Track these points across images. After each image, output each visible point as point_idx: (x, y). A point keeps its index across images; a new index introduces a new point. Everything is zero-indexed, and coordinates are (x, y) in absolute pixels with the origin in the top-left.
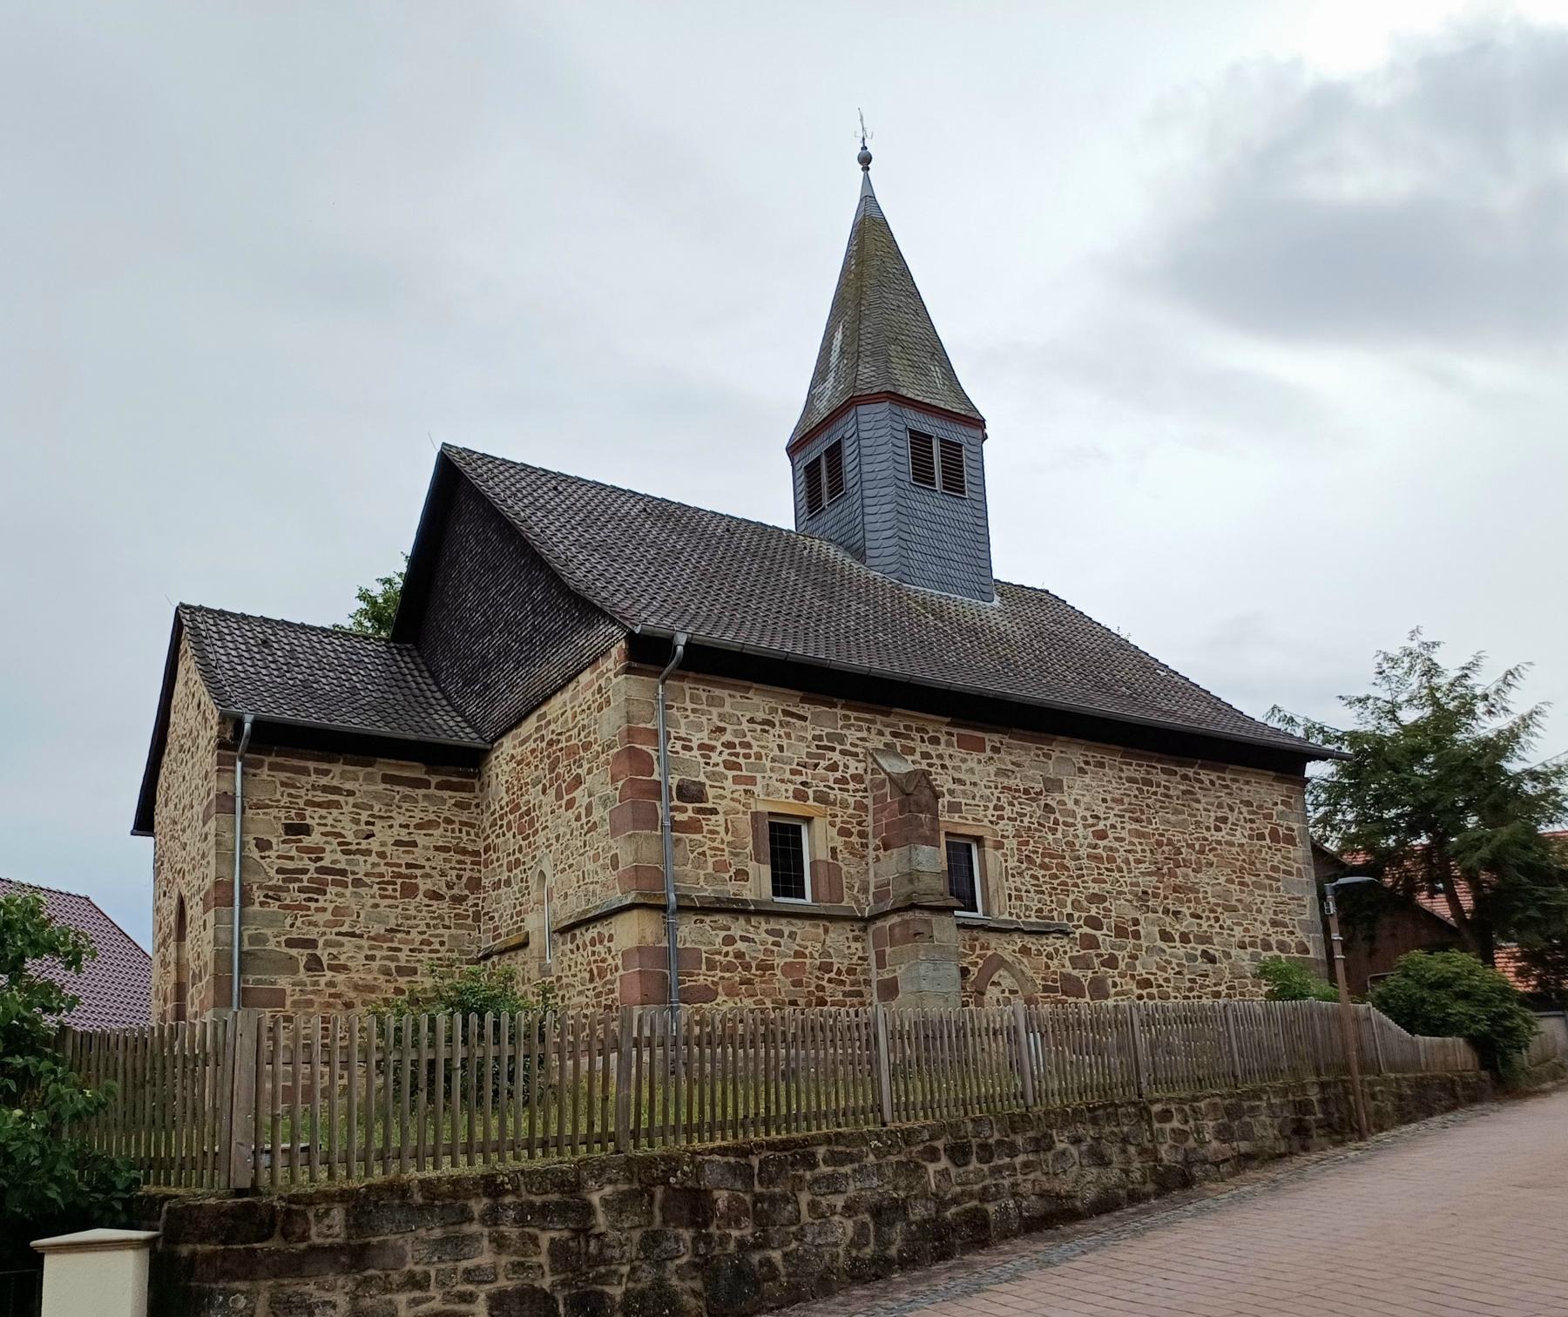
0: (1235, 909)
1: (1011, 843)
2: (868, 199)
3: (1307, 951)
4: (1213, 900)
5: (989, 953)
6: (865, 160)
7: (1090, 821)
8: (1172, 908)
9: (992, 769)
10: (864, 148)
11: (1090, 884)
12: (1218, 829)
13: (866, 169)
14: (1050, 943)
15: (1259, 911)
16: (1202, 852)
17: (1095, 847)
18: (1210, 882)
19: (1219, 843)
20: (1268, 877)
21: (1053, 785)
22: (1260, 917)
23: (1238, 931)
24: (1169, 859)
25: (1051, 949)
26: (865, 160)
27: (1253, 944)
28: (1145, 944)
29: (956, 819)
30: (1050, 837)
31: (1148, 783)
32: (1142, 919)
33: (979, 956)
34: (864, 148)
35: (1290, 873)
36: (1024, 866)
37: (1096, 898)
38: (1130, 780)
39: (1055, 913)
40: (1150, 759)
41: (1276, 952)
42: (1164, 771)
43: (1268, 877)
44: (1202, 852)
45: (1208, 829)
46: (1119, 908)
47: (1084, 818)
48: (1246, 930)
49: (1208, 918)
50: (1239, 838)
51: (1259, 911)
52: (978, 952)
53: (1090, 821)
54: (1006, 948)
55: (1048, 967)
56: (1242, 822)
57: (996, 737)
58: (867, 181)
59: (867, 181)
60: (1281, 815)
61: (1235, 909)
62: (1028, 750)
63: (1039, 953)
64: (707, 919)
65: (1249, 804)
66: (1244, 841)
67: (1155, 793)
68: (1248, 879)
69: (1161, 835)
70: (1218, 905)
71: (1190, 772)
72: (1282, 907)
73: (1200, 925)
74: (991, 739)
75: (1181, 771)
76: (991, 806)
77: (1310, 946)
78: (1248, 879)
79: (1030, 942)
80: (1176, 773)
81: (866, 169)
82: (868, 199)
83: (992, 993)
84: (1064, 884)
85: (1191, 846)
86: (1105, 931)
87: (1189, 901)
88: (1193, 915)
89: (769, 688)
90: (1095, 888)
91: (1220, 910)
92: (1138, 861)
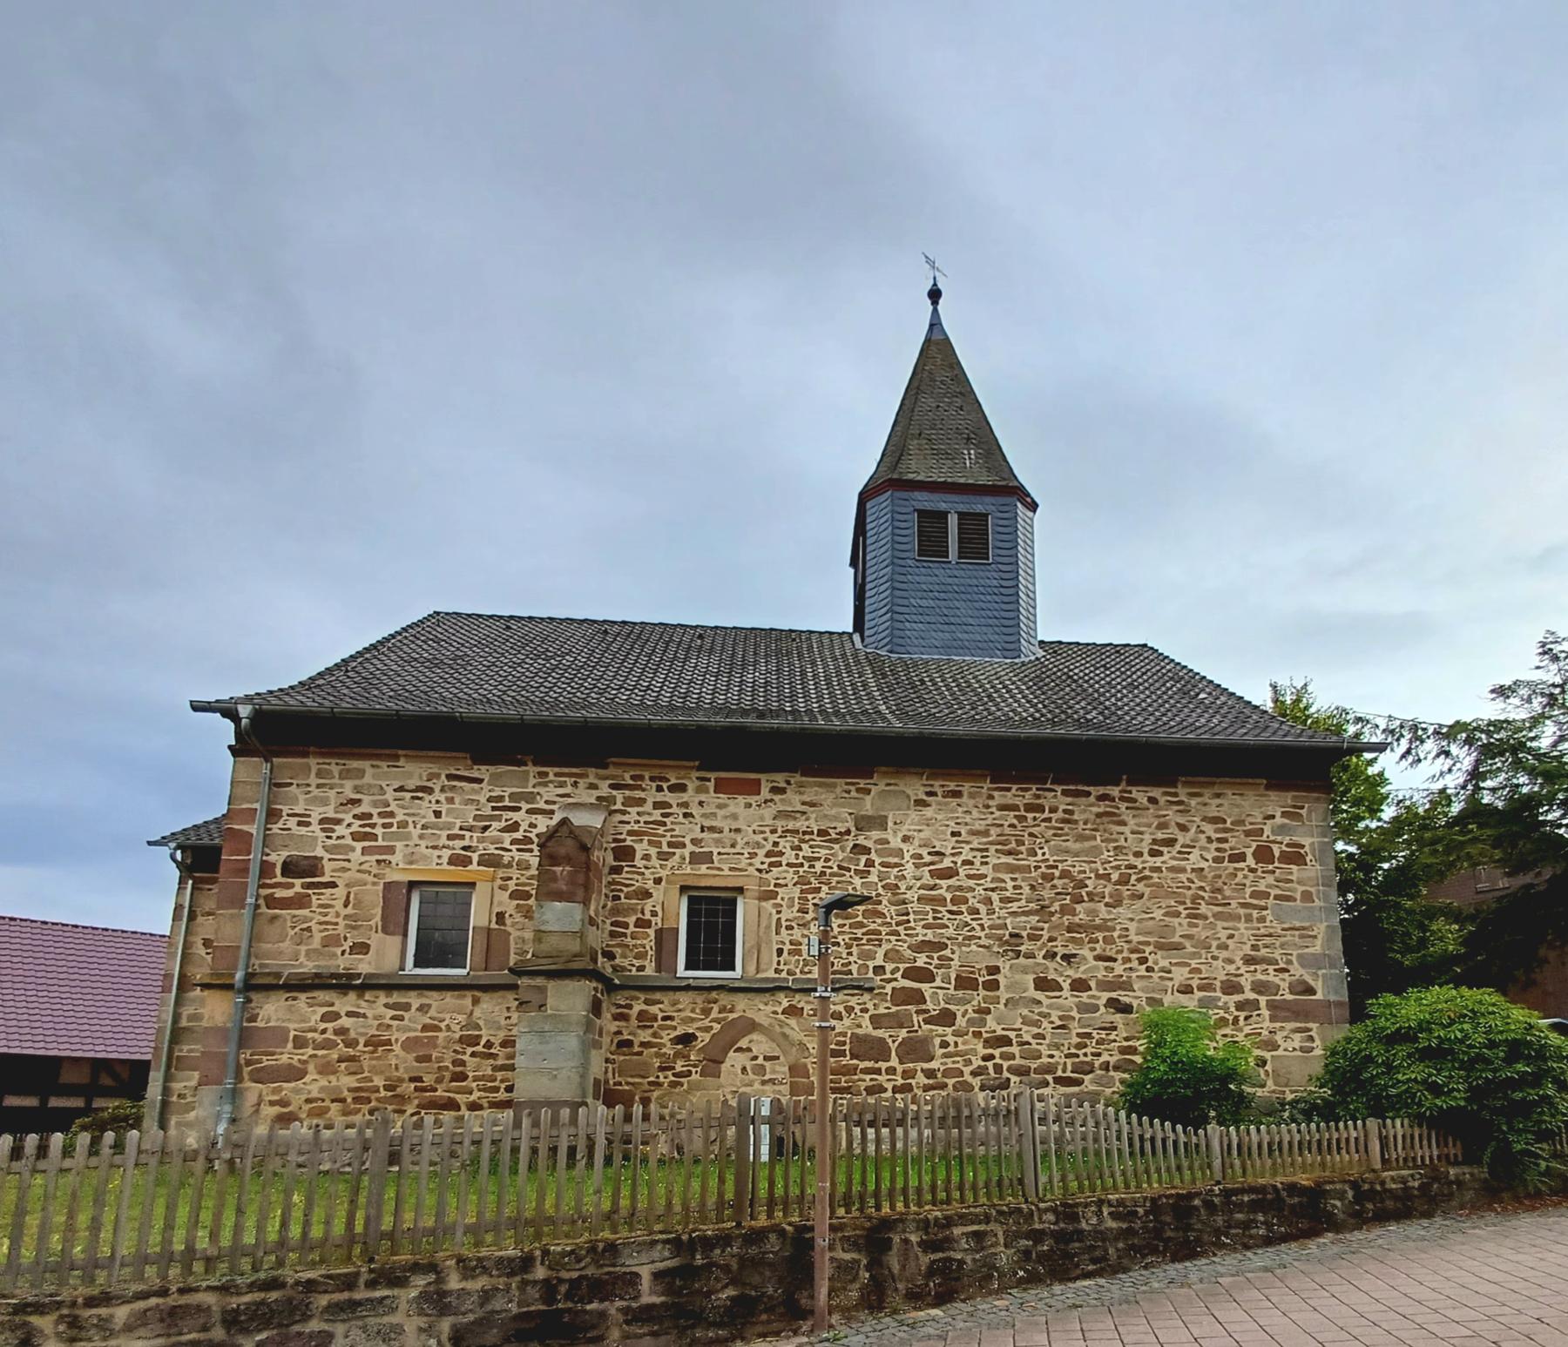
6: (935, 295)
16: (1124, 880)
22: (1224, 954)
26: (935, 295)
58: (935, 311)
59: (935, 311)
83: (734, 1060)
88: (1098, 958)
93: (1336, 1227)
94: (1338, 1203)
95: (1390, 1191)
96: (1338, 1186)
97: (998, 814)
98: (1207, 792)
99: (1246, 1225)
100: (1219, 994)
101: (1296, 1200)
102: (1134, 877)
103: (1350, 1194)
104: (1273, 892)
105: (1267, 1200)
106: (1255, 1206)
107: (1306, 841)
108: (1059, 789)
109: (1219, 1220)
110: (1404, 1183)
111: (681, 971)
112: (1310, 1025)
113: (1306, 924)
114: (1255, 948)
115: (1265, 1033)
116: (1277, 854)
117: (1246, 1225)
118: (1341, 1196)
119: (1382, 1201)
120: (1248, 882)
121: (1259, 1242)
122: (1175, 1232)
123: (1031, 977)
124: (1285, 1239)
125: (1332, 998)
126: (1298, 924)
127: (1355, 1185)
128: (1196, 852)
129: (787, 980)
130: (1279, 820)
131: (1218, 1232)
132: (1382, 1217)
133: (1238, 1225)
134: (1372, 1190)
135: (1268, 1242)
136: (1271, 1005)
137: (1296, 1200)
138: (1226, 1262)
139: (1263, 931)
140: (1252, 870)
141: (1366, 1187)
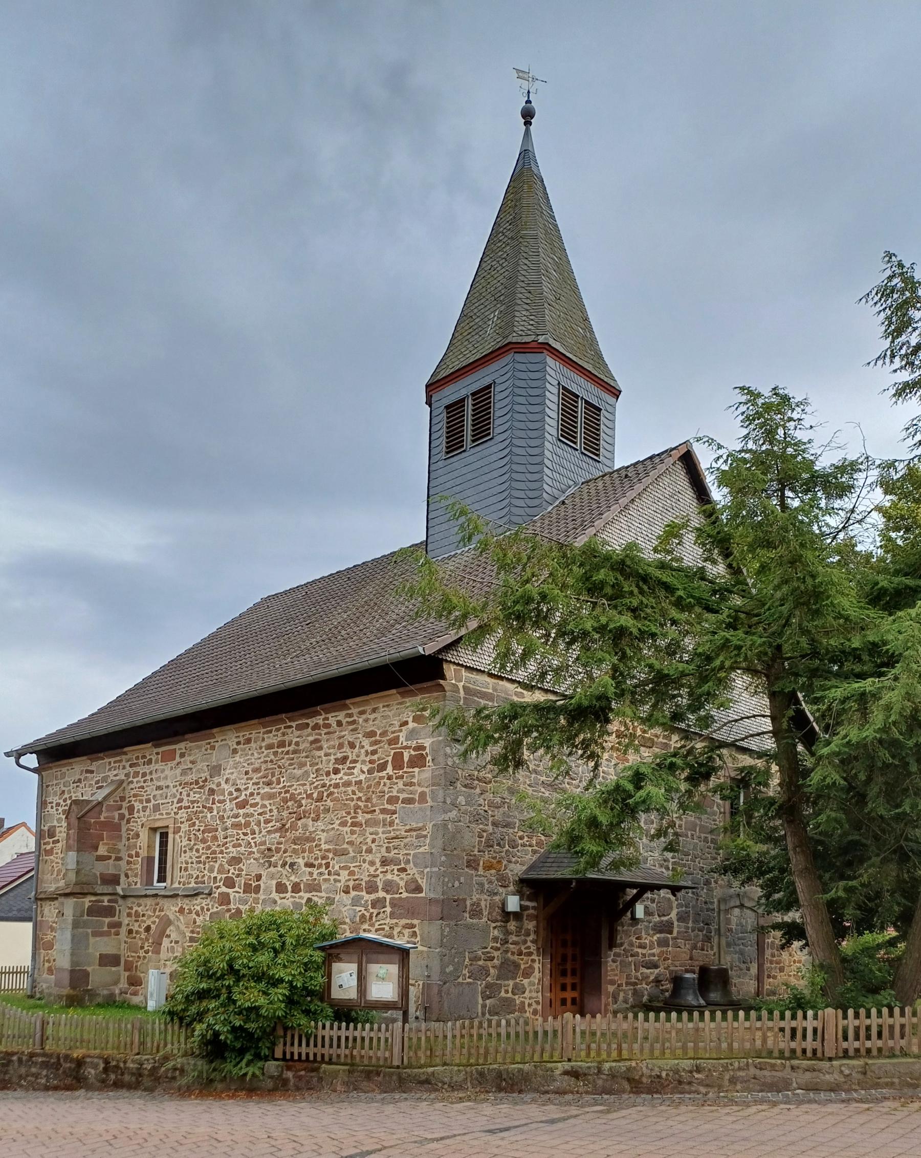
0: (344, 853)
1: (185, 827)
2: (526, 157)
3: (419, 889)
4: (324, 847)
5: (163, 913)
6: (528, 115)
7: (235, 794)
8: (289, 860)
9: (178, 771)
10: (528, 102)
11: (231, 849)
12: (336, 771)
13: (528, 123)
14: (198, 903)
15: (369, 851)
16: (320, 799)
17: (236, 816)
18: (322, 831)
19: (337, 786)
20: (383, 811)
21: (216, 770)
22: (369, 857)
23: (344, 874)
24: (293, 811)
25: (198, 908)
26: (528, 115)
27: (356, 888)
28: (262, 897)
29: (158, 817)
30: (209, 815)
31: (282, 744)
32: (264, 874)
33: (158, 917)
34: (528, 102)
35: (409, 801)
36: (192, 843)
37: (235, 861)
38: (269, 747)
39: (206, 878)
40: (282, 721)
41: (381, 894)
42: (299, 728)
43: (383, 811)
44: (320, 799)
45: (328, 774)
46: (250, 867)
47: (230, 794)
48: (352, 873)
49: (320, 866)
50: (359, 773)
51: (369, 851)
52: (157, 913)
53: (235, 794)
54: (171, 909)
55: (195, 922)
56: (362, 757)
57: (182, 745)
58: (527, 134)
59: (527, 134)
60: (412, 734)
61: (344, 853)
62: (199, 747)
63: (190, 912)
64: (52, 903)
65: (371, 734)
66: (362, 777)
67: (287, 753)
68: (361, 818)
69: (286, 792)
70: (328, 851)
71: (319, 720)
72: (396, 842)
73: (311, 874)
74: (180, 747)
75: (311, 722)
76: (175, 800)
77: (423, 883)
78: (361, 818)
79: (186, 904)
80: (308, 724)
81: (528, 123)
82: (526, 157)
83: (166, 942)
84: (214, 852)
85: (309, 796)
86: (237, 889)
87: (304, 851)
88: (307, 865)
89: (243, 724)
90: (233, 852)
91: (331, 855)
92: (267, 822)
93: (89, 1087)
94: (93, 1072)
95: (128, 1068)
96: (96, 1060)
97: (266, 752)
98: (368, 708)
99: (37, 1076)
100: (364, 893)
101: (68, 1065)
102: (325, 794)
103: (102, 1066)
104: (402, 796)
105: (53, 1063)
106: (45, 1065)
107: (427, 742)
108: (294, 724)
109: (23, 1070)
110: (142, 1065)
111: (155, 884)
112: (415, 922)
113: (420, 825)
114: (388, 850)
115: (387, 928)
116: (406, 759)
117: (37, 1076)
118: (95, 1067)
119: (122, 1074)
120: (386, 789)
121: (42, 1087)
122: (68, 1075)
123: (274, 882)
124: (56, 1088)
125: (432, 896)
126: (414, 825)
127: (107, 1062)
128: (358, 765)
129: (178, 889)
130: (411, 725)
131: (21, 1077)
132: (118, 1085)
133: (33, 1075)
134: (117, 1067)
135: (47, 1088)
136: (393, 904)
137: (68, 1065)
138: (19, 1093)
139: (392, 834)
140: (390, 778)
141: (114, 1063)
